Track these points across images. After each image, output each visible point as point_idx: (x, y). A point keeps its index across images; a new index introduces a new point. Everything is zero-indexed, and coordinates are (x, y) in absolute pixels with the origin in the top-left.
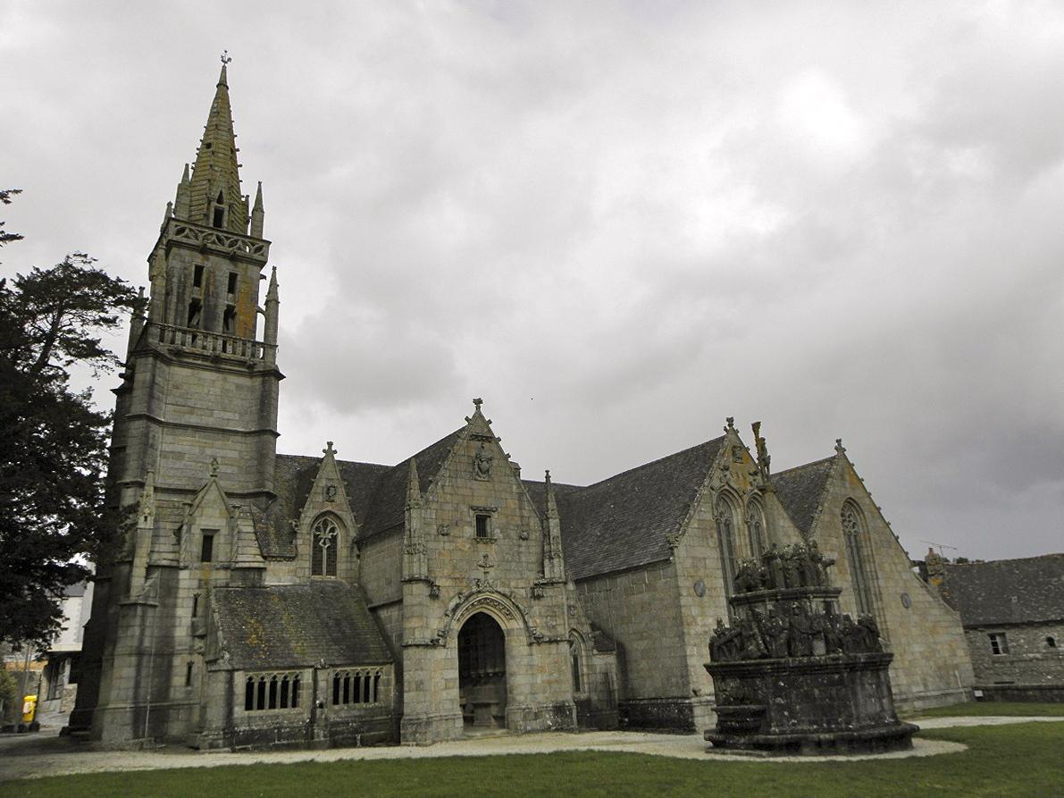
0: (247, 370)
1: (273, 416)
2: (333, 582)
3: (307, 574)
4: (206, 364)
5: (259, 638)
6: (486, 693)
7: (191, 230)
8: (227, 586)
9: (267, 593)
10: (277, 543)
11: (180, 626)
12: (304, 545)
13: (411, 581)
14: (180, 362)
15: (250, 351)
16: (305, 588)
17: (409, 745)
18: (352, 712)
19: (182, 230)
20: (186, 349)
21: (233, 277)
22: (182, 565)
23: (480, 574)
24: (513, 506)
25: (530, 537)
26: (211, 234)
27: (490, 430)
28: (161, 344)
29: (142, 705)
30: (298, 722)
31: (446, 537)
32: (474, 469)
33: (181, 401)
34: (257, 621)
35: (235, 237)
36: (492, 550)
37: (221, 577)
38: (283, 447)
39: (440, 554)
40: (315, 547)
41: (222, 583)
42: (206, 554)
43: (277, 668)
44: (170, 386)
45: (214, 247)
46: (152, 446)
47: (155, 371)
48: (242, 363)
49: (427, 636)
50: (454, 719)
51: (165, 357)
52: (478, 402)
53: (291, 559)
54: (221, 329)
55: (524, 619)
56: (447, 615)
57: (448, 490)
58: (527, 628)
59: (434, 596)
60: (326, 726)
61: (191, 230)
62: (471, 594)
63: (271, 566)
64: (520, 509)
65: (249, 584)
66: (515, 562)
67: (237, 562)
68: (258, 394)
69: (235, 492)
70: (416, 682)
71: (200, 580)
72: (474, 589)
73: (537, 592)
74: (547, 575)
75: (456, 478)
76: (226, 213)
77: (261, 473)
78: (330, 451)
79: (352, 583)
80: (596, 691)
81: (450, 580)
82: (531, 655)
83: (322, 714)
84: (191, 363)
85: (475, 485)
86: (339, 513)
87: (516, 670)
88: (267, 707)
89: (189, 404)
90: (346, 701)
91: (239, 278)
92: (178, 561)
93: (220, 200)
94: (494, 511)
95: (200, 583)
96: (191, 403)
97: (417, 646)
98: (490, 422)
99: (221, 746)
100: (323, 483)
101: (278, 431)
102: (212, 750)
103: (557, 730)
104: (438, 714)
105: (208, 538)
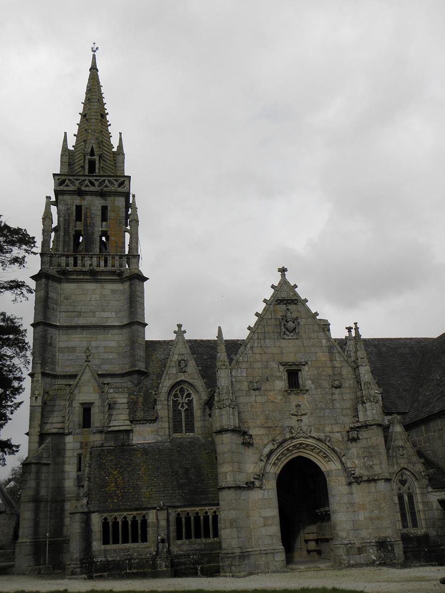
0: (118, 278)
1: (139, 311)
2: (191, 438)
3: (167, 433)
4: (86, 277)
5: (117, 486)
6: (310, 532)
7: (69, 180)
8: (102, 446)
9: (134, 449)
10: (142, 411)
11: (68, 479)
12: (163, 410)
13: (221, 431)
14: (68, 279)
15: (118, 262)
16: (166, 444)
17: (226, 576)
18: (193, 546)
19: (64, 181)
20: (71, 268)
21: (104, 209)
22: (66, 431)
23: (293, 422)
24: (323, 359)
25: (343, 385)
26: (85, 180)
27: (296, 294)
28: (51, 268)
29: (42, 540)
30: (146, 554)
31: (257, 392)
32: (281, 329)
33: (71, 308)
34: (119, 472)
35: (103, 178)
36: (304, 401)
37: (97, 439)
38: (151, 334)
39: (252, 406)
40: (174, 411)
41: (97, 444)
42: (86, 422)
43: (125, 510)
44: (62, 298)
45: (87, 189)
46: (51, 344)
47: (48, 288)
48: (113, 273)
49: (242, 480)
50: (273, 553)
51: (55, 277)
52: (283, 270)
53: (154, 421)
54: (98, 250)
55: (341, 461)
56: (261, 460)
57: (256, 350)
58: (345, 468)
59: (248, 444)
60: (167, 558)
61: (69, 180)
62: (285, 441)
63: (138, 428)
64: (331, 361)
65: (119, 444)
66: (330, 409)
67: (110, 427)
68: (127, 295)
69: (116, 373)
70: (230, 520)
71: (81, 443)
72: (288, 436)
73: (354, 434)
74: (361, 419)
75: (265, 339)
76: (97, 162)
77: (133, 356)
78: (180, 332)
79: (206, 438)
80: (434, 527)
81: (262, 429)
82: (352, 494)
83: (163, 548)
84: (76, 279)
85: (284, 343)
86: (191, 381)
87: (337, 508)
88: (130, 541)
89: (77, 310)
90: (188, 537)
91: (109, 209)
92: (63, 429)
93: (92, 153)
94: (304, 365)
95: (81, 445)
96: (78, 309)
97: (229, 488)
98: (295, 286)
99: (78, 573)
100: (176, 358)
101: (146, 321)
102: (73, 577)
103: (380, 564)
104: (258, 549)
105: (87, 409)
